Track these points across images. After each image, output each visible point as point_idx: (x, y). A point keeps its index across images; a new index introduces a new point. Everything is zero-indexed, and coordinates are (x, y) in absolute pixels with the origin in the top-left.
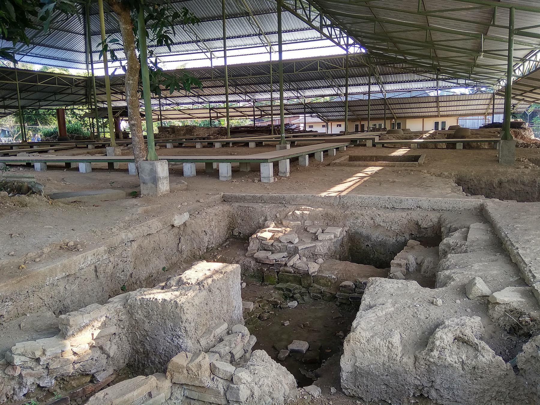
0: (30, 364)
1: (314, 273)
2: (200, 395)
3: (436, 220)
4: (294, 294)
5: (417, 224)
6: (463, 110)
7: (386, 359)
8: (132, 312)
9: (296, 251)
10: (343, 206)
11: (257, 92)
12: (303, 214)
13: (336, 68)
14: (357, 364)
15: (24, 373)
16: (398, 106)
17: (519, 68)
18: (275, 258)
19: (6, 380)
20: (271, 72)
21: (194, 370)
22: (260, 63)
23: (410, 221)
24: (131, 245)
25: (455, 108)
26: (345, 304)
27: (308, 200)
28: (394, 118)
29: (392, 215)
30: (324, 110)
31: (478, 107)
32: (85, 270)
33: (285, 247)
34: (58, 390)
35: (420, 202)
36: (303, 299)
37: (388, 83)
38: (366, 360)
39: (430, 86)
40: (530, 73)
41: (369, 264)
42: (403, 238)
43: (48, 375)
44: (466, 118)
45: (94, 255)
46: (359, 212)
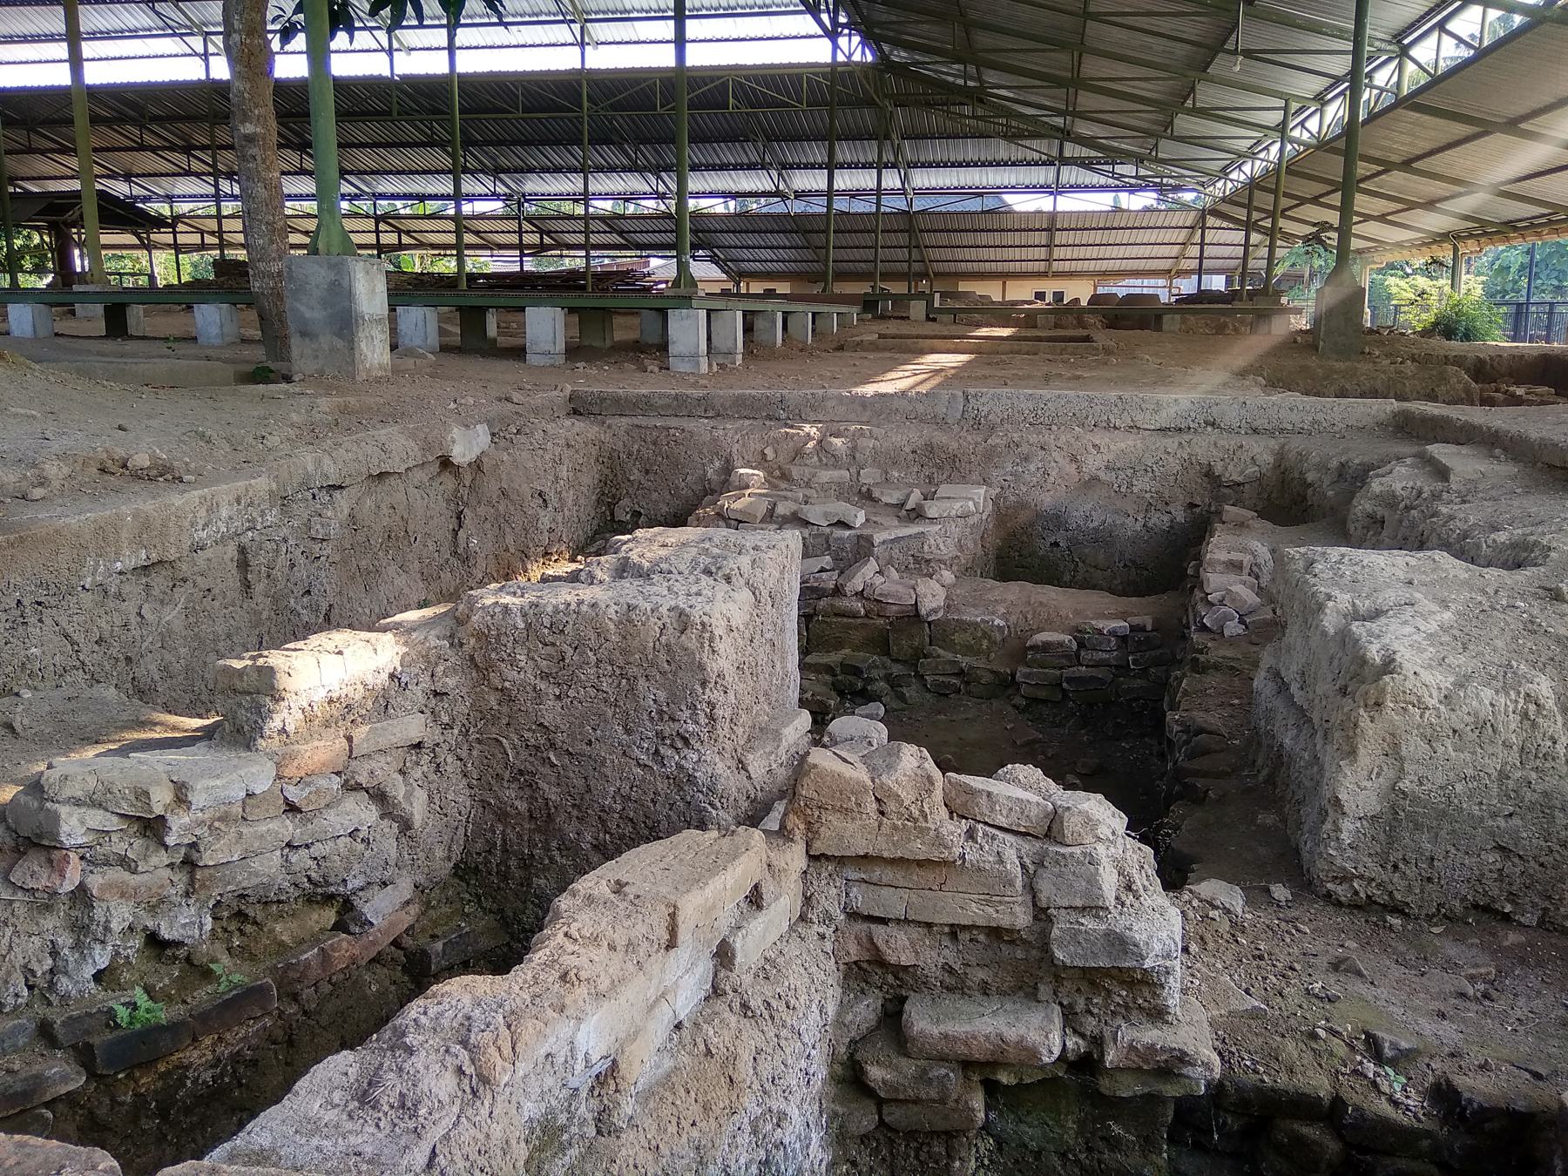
0: (119, 847)
1: (935, 611)
2: (914, 898)
3: (1267, 459)
4: (871, 680)
6: (1114, 257)
7: (1514, 757)
8: (487, 659)
9: (863, 548)
10: (977, 424)
11: (531, 170)
13: (787, 105)
14: (1405, 785)
15: (95, 882)
16: (942, 238)
17: (1302, 123)
19: (20, 910)
20: (586, 104)
21: (907, 796)
22: (549, 72)
23: (1187, 464)
24: (331, 502)
26: (1044, 701)
28: (925, 275)
30: (730, 239)
32: (208, 553)
33: (821, 540)
34: (225, 959)
35: (1214, 409)
36: (902, 698)
37: (923, 166)
38: (1435, 770)
39: (1034, 182)
41: (1086, 585)
42: (1166, 518)
43: (187, 894)
45: (238, 502)
46: (1033, 438)
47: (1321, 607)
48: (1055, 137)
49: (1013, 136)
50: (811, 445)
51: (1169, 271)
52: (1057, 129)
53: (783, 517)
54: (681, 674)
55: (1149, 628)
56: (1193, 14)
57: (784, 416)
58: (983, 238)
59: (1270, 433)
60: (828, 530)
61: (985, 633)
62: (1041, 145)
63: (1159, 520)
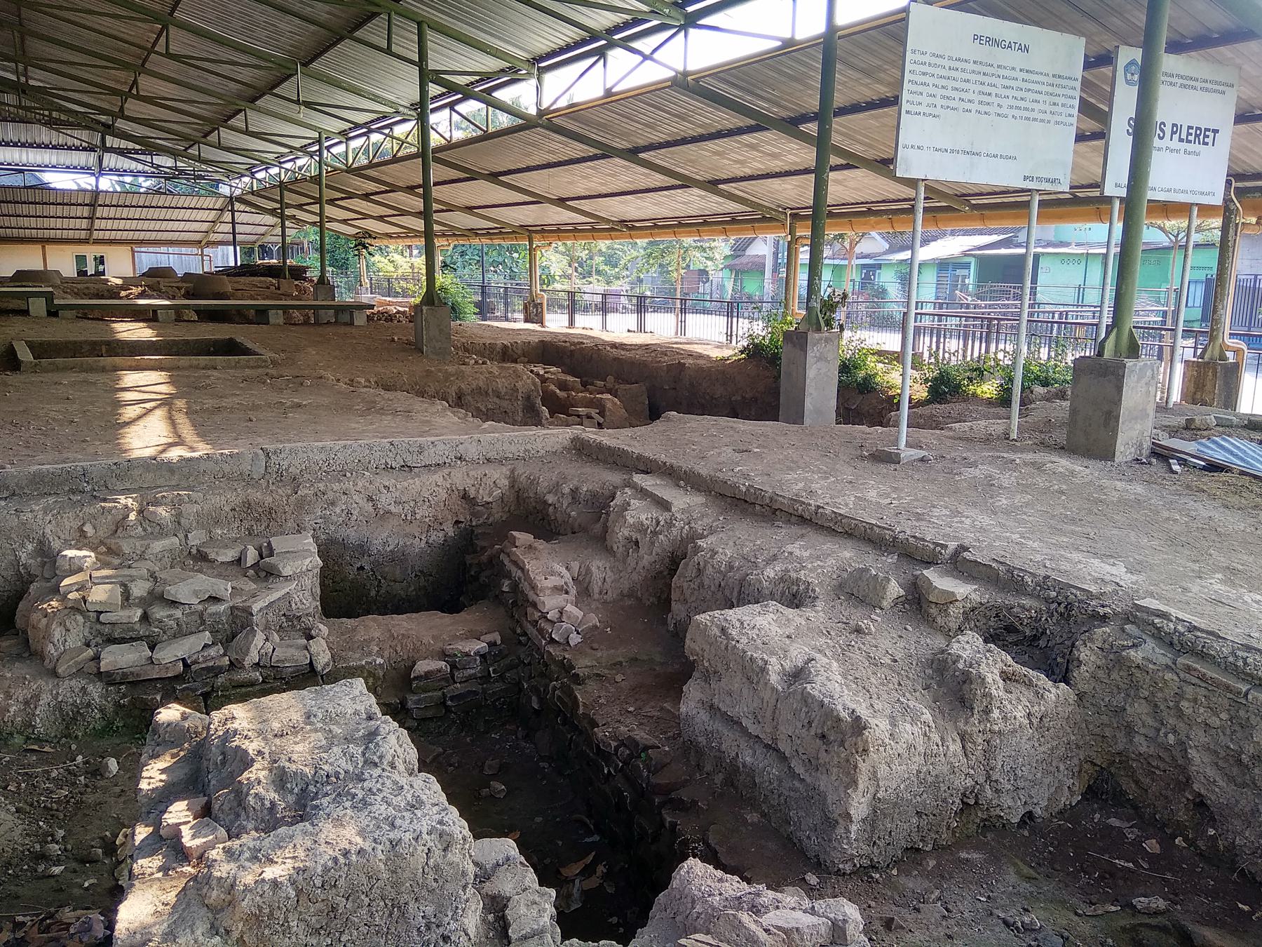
5: (465, 496)
18: (180, 655)
25: (158, 225)
29: (415, 484)
31: (189, 226)
44: (157, 250)
47: (763, 670)
49: (51, 123)
50: (132, 516)
53: (141, 599)
55: (499, 642)
57: (89, 488)
58: (25, 209)
59: (501, 462)
60: (200, 607)
61: (369, 672)
62: (84, 135)
63: (437, 537)
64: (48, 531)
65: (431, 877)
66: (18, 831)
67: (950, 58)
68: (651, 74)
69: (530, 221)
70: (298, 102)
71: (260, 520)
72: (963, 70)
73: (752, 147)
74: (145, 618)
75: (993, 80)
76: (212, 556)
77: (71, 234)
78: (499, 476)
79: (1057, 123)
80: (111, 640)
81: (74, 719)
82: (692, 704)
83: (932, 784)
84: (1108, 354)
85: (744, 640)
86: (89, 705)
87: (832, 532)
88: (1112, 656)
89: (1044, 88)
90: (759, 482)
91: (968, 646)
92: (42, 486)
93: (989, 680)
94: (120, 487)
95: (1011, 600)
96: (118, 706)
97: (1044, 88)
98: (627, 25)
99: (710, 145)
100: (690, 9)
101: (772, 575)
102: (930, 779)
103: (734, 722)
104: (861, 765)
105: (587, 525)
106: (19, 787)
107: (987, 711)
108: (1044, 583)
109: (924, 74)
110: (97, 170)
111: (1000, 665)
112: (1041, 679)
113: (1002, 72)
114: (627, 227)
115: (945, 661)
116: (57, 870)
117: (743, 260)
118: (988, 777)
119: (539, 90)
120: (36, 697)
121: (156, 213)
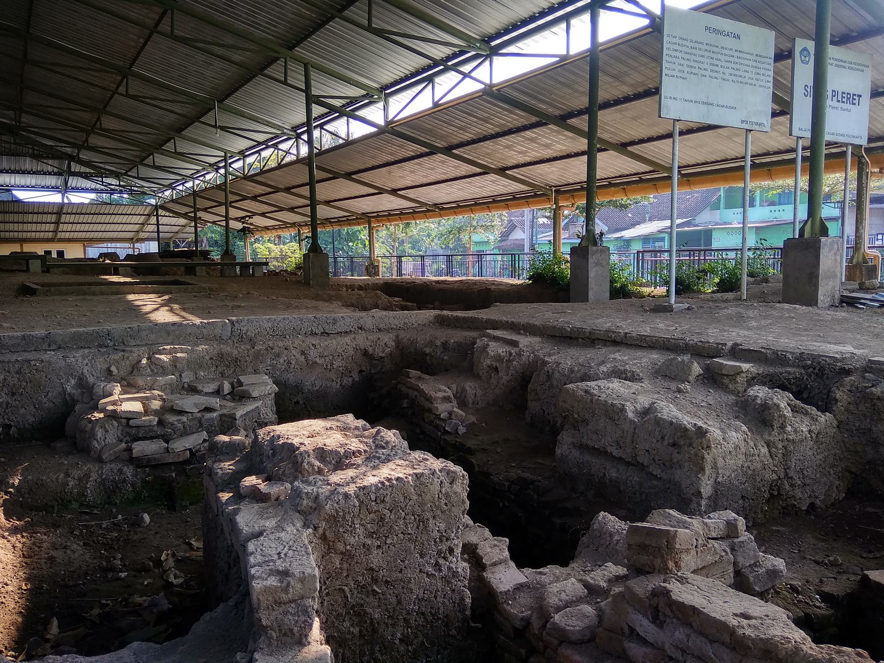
5: (365, 353)
12: (175, 360)
18: (188, 446)
27: (168, 333)
29: (333, 344)
33: (196, 422)
40: (262, 172)
42: (350, 379)
47: (623, 410)
48: (62, 158)
49: (37, 157)
50: (144, 361)
51: (132, 239)
52: (66, 154)
54: (454, 509)
56: (183, 103)
57: (111, 344)
59: (388, 330)
60: (199, 415)
63: (348, 381)
64: (85, 371)
65: (443, 501)
66: (87, 557)
67: (691, 41)
68: (469, 87)
69: (369, 209)
70: (215, 127)
71: (229, 365)
72: (700, 49)
73: (532, 140)
74: (161, 423)
75: (719, 56)
76: (200, 387)
77: (42, 235)
78: (388, 339)
79: (761, 86)
80: (136, 439)
81: (114, 492)
82: (565, 447)
83: (751, 476)
84: (807, 235)
85: (604, 395)
86: (124, 481)
87: (640, 347)
88: (858, 394)
89: (751, 63)
90: (578, 325)
91: (760, 392)
92: (80, 342)
93: (782, 405)
94: (132, 343)
95: (779, 370)
96: (145, 482)
97: (751, 63)
98: (455, 56)
99: (503, 141)
100: (493, 44)
101: (605, 370)
102: (750, 472)
103: (601, 452)
104: (706, 456)
105: (461, 362)
106: (81, 532)
107: (783, 427)
108: (801, 357)
109: (676, 50)
110: (62, 188)
111: (786, 399)
112: (813, 411)
113: (724, 51)
114: (438, 209)
115: (747, 401)
116: (123, 575)
117: (508, 243)
118: (786, 474)
119: (385, 109)
120: (87, 476)
121: (103, 219)
